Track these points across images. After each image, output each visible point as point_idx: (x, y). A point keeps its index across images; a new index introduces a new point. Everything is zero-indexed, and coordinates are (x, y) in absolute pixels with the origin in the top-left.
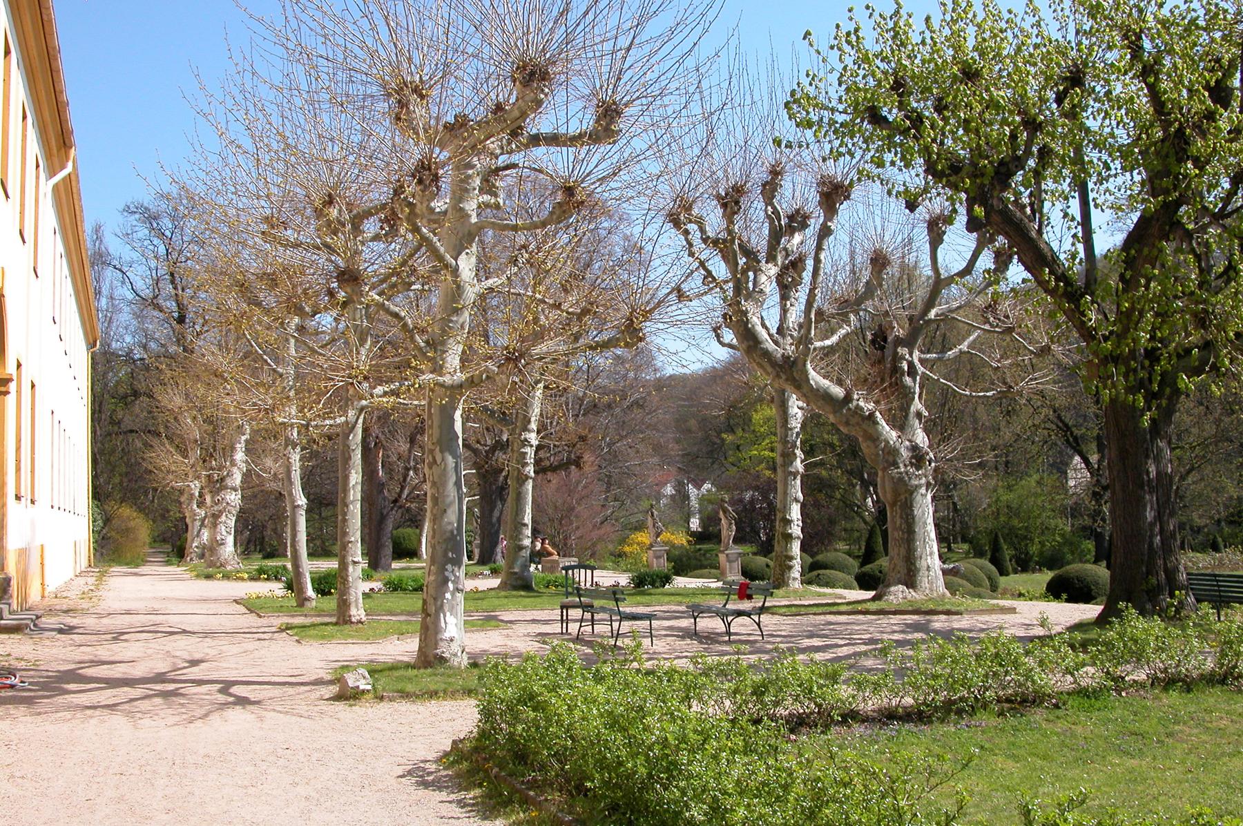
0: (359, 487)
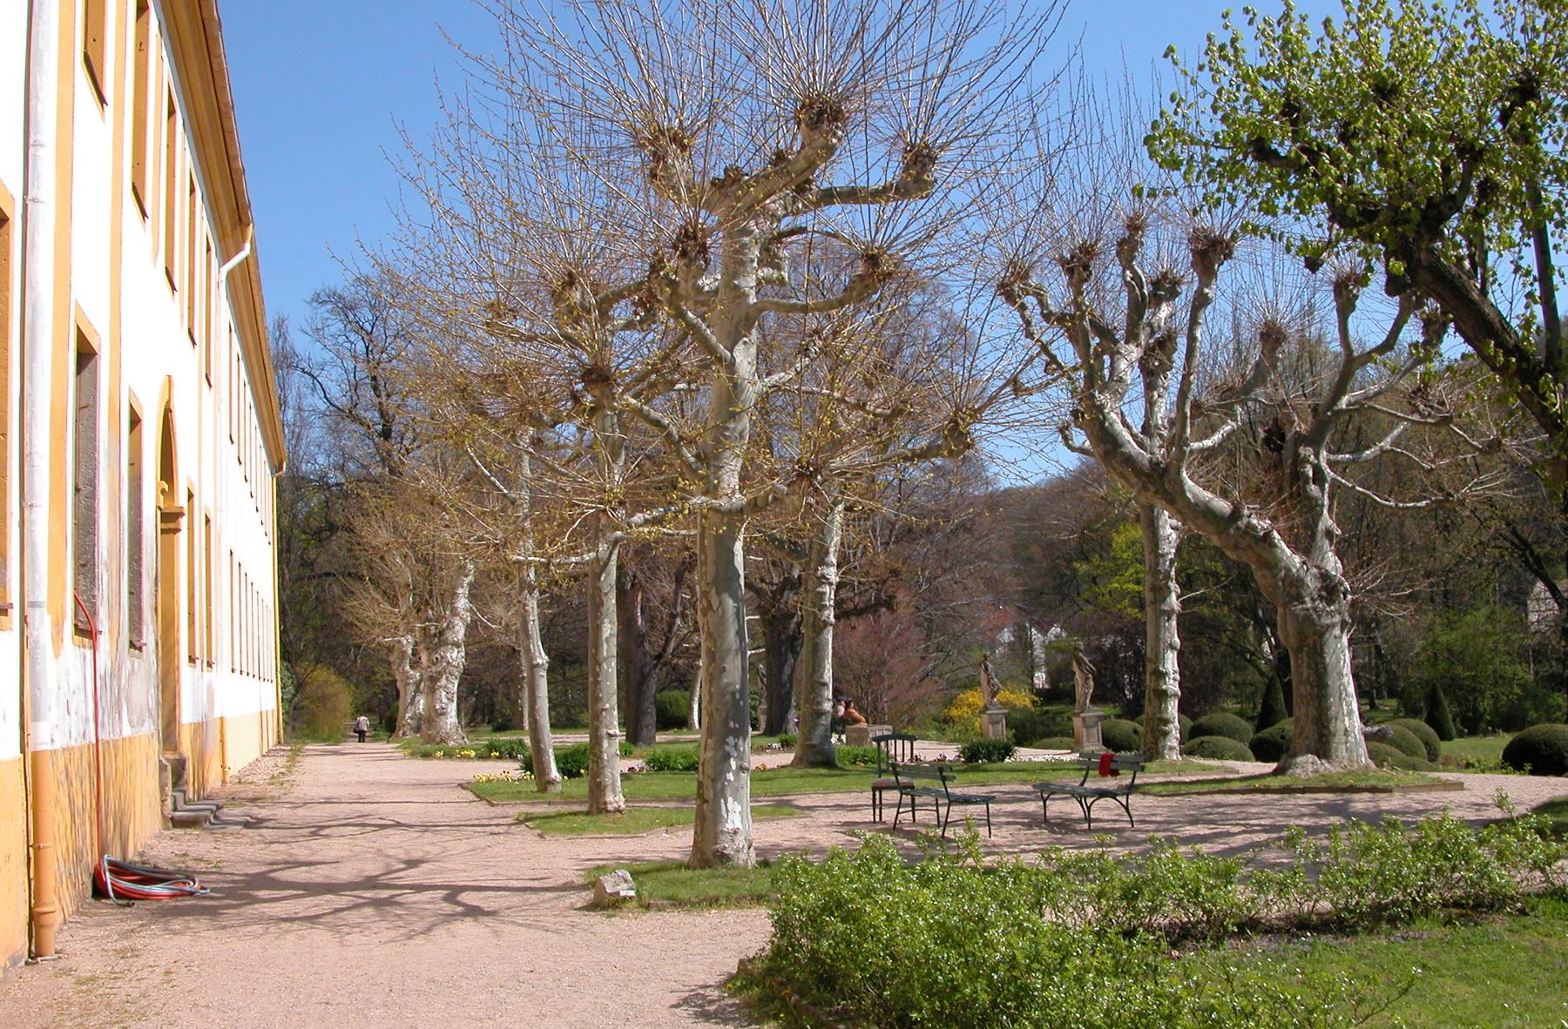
0: (614, 640)
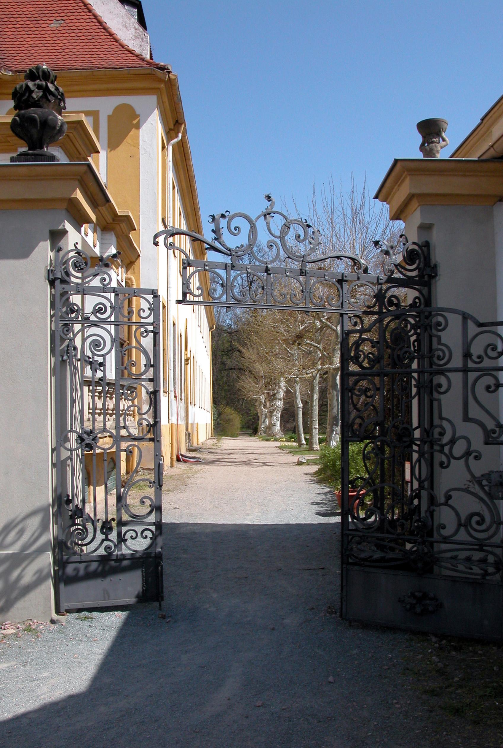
0: (317, 400)
